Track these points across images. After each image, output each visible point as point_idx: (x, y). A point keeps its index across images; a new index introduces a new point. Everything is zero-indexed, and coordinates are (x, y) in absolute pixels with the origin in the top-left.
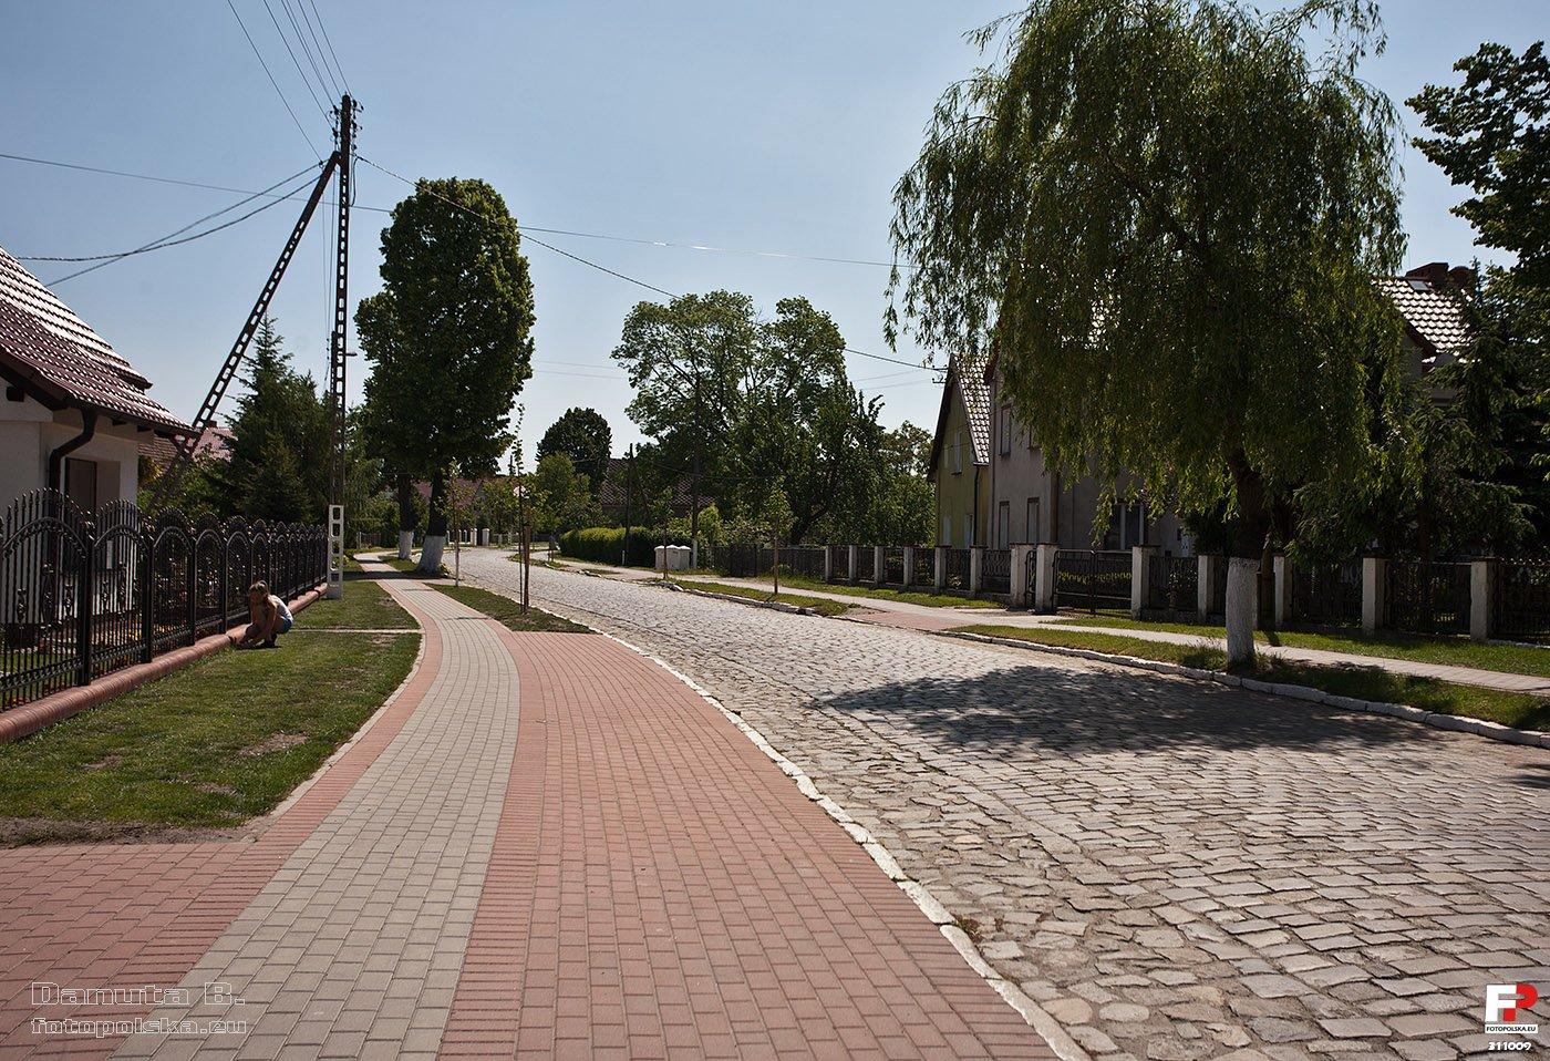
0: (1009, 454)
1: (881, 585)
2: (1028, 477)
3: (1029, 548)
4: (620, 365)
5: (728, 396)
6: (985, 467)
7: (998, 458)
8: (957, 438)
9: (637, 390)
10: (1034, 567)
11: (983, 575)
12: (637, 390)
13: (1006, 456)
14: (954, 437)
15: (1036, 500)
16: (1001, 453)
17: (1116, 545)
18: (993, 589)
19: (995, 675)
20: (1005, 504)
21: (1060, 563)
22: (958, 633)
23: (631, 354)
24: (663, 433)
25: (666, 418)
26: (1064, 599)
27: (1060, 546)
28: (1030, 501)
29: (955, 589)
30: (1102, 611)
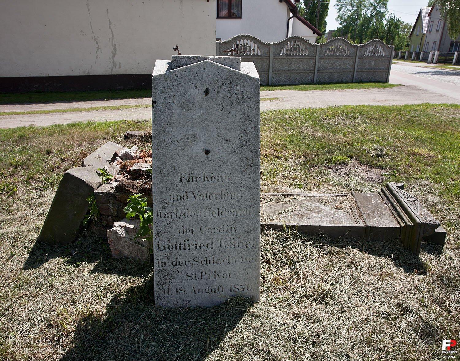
0: (431, 32)
1: (400, 59)
2: (436, 37)
3: (434, 52)
4: (335, 8)
5: (359, 15)
6: (425, 34)
7: (428, 33)
8: (418, 28)
9: (338, 14)
10: (434, 56)
11: (423, 56)
12: (338, 14)
13: (430, 32)
14: (418, 27)
15: (436, 42)
16: (429, 31)
17: (451, 51)
18: (425, 60)
19: (233, 324)
20: (428, 42)
21: (440, 55)
22: (420, 67)
23: (338, 5)
24: (343, 25)
25: (345, 21)
26: (440, 61)
27: (440, 51)
28: (434, 42)
29: (417, 59)
30: (449, 20)
